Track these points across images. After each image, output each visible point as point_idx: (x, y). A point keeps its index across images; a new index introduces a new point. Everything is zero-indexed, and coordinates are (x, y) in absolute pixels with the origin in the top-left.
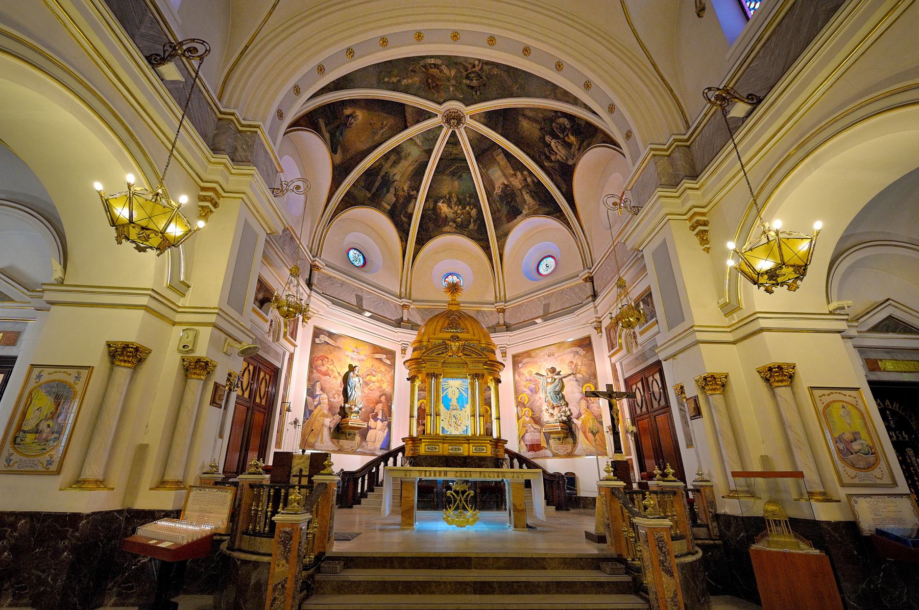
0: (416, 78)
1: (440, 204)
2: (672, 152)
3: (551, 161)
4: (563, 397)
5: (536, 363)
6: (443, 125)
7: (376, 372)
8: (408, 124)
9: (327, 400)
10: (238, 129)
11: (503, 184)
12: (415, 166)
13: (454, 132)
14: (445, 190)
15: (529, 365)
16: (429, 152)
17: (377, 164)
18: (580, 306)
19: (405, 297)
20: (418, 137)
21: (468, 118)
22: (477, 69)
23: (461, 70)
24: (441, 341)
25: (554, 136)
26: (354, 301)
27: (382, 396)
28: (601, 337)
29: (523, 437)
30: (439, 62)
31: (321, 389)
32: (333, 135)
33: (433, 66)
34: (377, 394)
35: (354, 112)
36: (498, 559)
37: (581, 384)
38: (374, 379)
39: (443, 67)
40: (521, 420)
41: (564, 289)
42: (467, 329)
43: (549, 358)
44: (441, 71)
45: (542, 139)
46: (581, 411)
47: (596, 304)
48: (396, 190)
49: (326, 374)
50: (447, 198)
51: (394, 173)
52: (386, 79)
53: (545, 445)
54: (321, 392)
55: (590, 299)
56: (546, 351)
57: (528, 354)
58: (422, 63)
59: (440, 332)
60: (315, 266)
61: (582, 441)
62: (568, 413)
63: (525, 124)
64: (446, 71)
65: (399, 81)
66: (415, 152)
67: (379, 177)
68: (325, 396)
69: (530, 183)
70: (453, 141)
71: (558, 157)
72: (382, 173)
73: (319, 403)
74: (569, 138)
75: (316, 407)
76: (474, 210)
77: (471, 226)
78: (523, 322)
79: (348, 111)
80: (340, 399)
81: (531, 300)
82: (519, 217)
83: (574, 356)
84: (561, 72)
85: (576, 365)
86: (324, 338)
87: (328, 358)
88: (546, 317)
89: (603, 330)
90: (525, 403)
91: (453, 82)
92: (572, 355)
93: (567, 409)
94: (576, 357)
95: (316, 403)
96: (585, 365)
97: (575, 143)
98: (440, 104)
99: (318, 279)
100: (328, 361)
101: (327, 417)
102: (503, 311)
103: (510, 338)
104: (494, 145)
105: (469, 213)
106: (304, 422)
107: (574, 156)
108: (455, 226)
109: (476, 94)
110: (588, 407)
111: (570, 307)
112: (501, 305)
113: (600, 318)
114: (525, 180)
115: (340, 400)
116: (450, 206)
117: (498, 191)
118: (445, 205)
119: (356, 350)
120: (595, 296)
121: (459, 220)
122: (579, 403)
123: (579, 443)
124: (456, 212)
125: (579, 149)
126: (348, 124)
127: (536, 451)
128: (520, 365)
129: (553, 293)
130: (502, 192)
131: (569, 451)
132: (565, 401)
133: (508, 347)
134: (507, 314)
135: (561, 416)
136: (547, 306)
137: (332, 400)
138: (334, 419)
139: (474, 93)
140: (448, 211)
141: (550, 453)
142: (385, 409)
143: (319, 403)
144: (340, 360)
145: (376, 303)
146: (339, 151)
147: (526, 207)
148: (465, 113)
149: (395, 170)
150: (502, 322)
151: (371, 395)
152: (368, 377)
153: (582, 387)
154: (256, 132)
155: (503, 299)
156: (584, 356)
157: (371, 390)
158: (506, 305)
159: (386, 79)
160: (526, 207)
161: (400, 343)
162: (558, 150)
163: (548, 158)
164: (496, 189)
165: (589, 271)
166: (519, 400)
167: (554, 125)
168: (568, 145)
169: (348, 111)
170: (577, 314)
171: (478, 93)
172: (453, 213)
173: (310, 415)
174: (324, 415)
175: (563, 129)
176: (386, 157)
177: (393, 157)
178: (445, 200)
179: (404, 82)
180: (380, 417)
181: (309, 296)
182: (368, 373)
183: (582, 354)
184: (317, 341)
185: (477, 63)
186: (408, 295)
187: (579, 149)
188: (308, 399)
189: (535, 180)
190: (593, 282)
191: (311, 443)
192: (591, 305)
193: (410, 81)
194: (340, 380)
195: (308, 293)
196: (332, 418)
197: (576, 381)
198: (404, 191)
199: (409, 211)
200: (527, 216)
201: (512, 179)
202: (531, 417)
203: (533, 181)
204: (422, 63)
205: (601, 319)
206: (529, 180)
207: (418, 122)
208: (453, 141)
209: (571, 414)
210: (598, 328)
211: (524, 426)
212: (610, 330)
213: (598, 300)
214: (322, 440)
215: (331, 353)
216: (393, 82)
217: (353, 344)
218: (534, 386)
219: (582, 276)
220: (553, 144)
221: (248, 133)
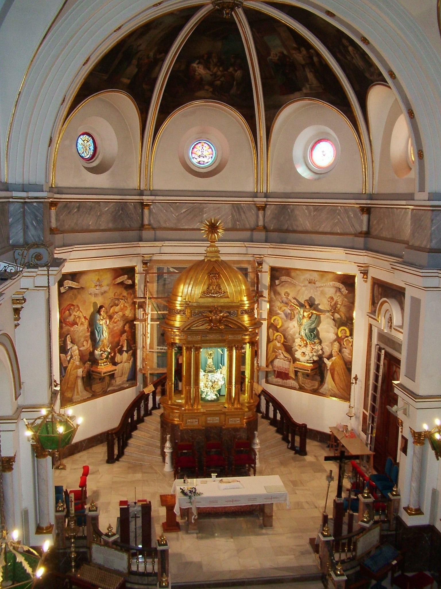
1: (195, 65)
3: (346, 58)
4: (317, 336)
5: (294, 285)
7: (118, 299)
9: (77, 351)
11: (283, 53)
15: (287, 285)
27: (125, 325)
29: (272, 362)
31: (72, 342)
34: (121, 324)
36: (258, 581)
37: (337, 325)
38: (117, 309)
40: (271, 345)
43: (309, 285)
46: (333, 353)
49: (75, 323)
50: (205, 58)
53: (293, 377)
54: (72, 345)
56: (308, 276)
57: (287, 272)
61: (329, 383)
62: (320, 352)
68: (76, 347)
73: (71, 357)
75: (69, 362)
77: (233, 91)
80: (87, 346)
82: (297, 94)
83: (336, 292)
85: (336, 303)
87: (73, 305)
90: (278, 327)
92: (333, 290)
93: (320, 347)
94: (338, 294)
95: (68, 359)
96: (345, 306)
100: (74, 308)
101: (79, 367)
102: (263, 208)
106: (61, 381)
108: (211, 90)
110: (340, 351)
114: (311, 57)
115: (88, 346)
116: (207, 67)
119: (98, 283)
121: (218, 83)
122: (332, 343)
123: (326, 383)
124: (214, 75)
127: (283, 379)
128: (277, 282)
130: (278, 60)
131: (316, 387)
132: (319, 339)
135: (313, 356)
137: (81, 349)
138: (85, 368)
140: (205, 72)
141: (297, 385)
142: (130, 337)
143: (71, 357)
144: (85, 302)
147: (308, 86)
150: (261, 223)
151: (116, 328)
152: (112, 308)
153: (338, 329)
156: (346, 296)
157: (116, 323)
160: (308, 86)
164: (272, 55)
166: (272, 321)
172: (211, 75)
173: (65, 372)
174: (77, 367)
180: (125, 349)
182: (111, 305)
183: (344, 293)
184: (62, 290)
188: (62, 356)
191: (69, 398)
194: (86, 323)
196: (83, 368)
197: (334, 320)
198: (148, 57)
199: (153, 76)
201: (294, 52)
202: (283, 344)
206: (315, 59)
209: (323, 353)
211: (274, 351)
214: (78, 392)
215: (76, 297)
218: (289, 312)
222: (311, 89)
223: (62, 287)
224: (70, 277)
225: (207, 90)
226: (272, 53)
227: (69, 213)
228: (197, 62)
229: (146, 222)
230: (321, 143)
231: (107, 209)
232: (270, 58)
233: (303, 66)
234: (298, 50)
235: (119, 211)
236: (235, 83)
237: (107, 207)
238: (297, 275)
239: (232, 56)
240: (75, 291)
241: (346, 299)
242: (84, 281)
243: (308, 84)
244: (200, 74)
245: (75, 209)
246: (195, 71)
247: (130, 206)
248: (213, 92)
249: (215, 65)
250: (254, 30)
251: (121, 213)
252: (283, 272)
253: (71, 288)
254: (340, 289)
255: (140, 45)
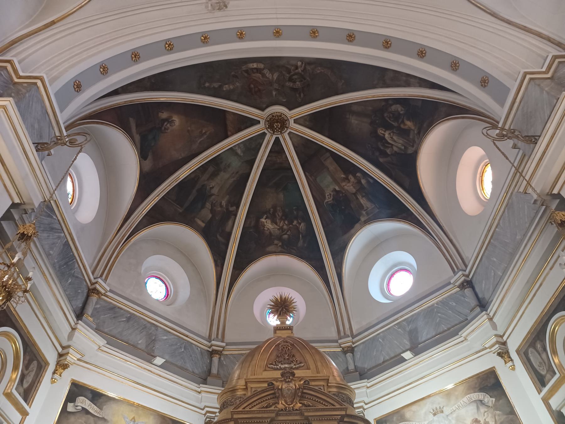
0: (238, 84)
1: (263, 220)
2: (555, 72)
6: (266, 132)
8: (229, 133)
10: (12, 80)
11: (335, 190)
12: (235, 179)
13: (277, 140)
14: (268, 203)
16: (251, 163)
17: (193, 176)
18: (466, 322)
19: (217, 339)
20: (239, 147)
21: (292, 121)
22: (300, 70)
23: (284, 73)
24: (266, 385)
25: (388, 127)
26: (141, 342)
28: (513, 369)
30: (261, 66)
32: (144, 139)
33: (255, 71)
35: (172, 117)
39: (266, 71)
41: (433, 305)
42: (306, 362)
43: (436, 418)
44: (264, 75)
45: (374, 133)
47: (491, 314)
48: (213, 205)
51: (211, 186)
52: (207, 85)
55: (478, 309)
56: (427, 407)
58: (244, 68)
59: (265, 370)
60: (95, 289)
63: (354, 121)
64: (269, 75)
65: (220, 87)
66: (235, 163)
67: (194, 191)
69: (365, 186)
70: (277, 148)
71: (395, 149)
72: (198, 186)
74: (405, 125)
76: (302, 224)
77: (300, 243)
78: (384, 362)
79: (164, 115)
81: (389, 328)
82: (357, 225)
83: (478, 408)
84: (390, 49)
86: (83, 402)
88: (416, 350)
89: (514, 355)
91: (276, 86)
92: (473, 407)
94: (483, 409)
97: (413, 128)
98: (263, 110)
99: (95, 309)
102: (351, 350)
103: (368, 390)
104: (321, 149)
105: (297, 228)
107: (414, 142)
108: (280, 244)
109: (300, 96)
111: (449, 329)
112: (347, 342)
113: (502, 337)
114: (359, 182)
116: (274, 222)
117: (329, 199)
118: (269, 221)
120: (483, 305)
121: (286, 236)
124: (281, 229)
125: (419, 133)
126: (163, 129)
129: (418, 314)
130: (333, 199)
133: (366, 407)
134: (358, 355)
136: (413, 335)
139: (298, 95)
140: (273, 227)
145: (174, 347)
146: (150, 157)
147: (364, 213)
148: (288, 116)
149: (213, 184)
150: (351, 367)
154: (35, 84)
155: (348, 332)
156: (495, 407)
158: (354, 340)
159: (207, 85)
160: (364, 213)
161: (204, 412)
162: (395, 141)
163: (384, 154)
164: (327, 197)
165: (464, 273)
167: (386, 115)
168: (404, 133)
169: (164, 115)
170: (464, 335)
171: (302, 95)
172: (278, 229)
175: (397, 117)
176: (203, 168)
177: (211, 169)
178: (269, 215)
179: (226, 88)
181: (73, 329)
184: (71, 407)
185: (299, 63)
186: (220, 337)
187: (419, 133)
189: (371, 181)
190: (473, 288)
192: (483, 317)
193: (232, 87)
195: (73, 324)
198: (221, 206)
199: (228, 229)
200: (368, 222)
201: (344, 184)
203: (368, 182)
204: (244, 68)
205: (505, 338)
206: (363, 181)
207: (240, 130)
208: (277, 148)
210: (504, 354)
212: (526, 354)
213: (492, 308)
216: (214, 87)
217: (128, 413)
219: (456, 281)
220: (387, 136)
221: (25, 85)
222: (367, 214)
223: (72, 404)
224: (90, 396)
225: (277, 245)
226: (326, 195)
227: (114, 317)
228: (265, 217)
229: (214, 371)
230: (395, 276)
231: (165, 338)
232: (326, 201)
233: (355, 194)
234: (347, 179)
235: (181, 348)
236: (301, 236)
237: (166, 336)
238: (414, 412)
239: (294, 208)
240: (92, 419)
241: (498, 412)
242: (108, 412)
243: (364, 211)
244: (268, 229)
245: (123, 318)
246: (264, 226)
247: (196, 350)
248: (282, 246)
249: (281, 219)
250: (307, 174)
251: (183, 352)
252: (395, 418)
253: (85, 411)
254: (481, 401)
255: (213, 187)
